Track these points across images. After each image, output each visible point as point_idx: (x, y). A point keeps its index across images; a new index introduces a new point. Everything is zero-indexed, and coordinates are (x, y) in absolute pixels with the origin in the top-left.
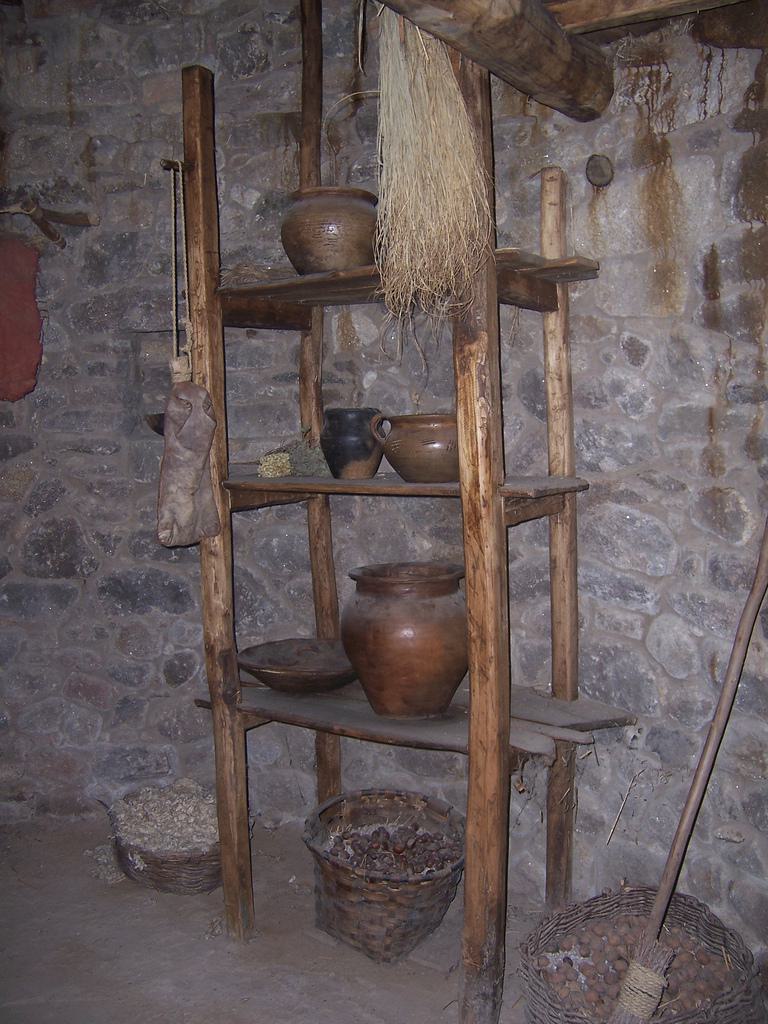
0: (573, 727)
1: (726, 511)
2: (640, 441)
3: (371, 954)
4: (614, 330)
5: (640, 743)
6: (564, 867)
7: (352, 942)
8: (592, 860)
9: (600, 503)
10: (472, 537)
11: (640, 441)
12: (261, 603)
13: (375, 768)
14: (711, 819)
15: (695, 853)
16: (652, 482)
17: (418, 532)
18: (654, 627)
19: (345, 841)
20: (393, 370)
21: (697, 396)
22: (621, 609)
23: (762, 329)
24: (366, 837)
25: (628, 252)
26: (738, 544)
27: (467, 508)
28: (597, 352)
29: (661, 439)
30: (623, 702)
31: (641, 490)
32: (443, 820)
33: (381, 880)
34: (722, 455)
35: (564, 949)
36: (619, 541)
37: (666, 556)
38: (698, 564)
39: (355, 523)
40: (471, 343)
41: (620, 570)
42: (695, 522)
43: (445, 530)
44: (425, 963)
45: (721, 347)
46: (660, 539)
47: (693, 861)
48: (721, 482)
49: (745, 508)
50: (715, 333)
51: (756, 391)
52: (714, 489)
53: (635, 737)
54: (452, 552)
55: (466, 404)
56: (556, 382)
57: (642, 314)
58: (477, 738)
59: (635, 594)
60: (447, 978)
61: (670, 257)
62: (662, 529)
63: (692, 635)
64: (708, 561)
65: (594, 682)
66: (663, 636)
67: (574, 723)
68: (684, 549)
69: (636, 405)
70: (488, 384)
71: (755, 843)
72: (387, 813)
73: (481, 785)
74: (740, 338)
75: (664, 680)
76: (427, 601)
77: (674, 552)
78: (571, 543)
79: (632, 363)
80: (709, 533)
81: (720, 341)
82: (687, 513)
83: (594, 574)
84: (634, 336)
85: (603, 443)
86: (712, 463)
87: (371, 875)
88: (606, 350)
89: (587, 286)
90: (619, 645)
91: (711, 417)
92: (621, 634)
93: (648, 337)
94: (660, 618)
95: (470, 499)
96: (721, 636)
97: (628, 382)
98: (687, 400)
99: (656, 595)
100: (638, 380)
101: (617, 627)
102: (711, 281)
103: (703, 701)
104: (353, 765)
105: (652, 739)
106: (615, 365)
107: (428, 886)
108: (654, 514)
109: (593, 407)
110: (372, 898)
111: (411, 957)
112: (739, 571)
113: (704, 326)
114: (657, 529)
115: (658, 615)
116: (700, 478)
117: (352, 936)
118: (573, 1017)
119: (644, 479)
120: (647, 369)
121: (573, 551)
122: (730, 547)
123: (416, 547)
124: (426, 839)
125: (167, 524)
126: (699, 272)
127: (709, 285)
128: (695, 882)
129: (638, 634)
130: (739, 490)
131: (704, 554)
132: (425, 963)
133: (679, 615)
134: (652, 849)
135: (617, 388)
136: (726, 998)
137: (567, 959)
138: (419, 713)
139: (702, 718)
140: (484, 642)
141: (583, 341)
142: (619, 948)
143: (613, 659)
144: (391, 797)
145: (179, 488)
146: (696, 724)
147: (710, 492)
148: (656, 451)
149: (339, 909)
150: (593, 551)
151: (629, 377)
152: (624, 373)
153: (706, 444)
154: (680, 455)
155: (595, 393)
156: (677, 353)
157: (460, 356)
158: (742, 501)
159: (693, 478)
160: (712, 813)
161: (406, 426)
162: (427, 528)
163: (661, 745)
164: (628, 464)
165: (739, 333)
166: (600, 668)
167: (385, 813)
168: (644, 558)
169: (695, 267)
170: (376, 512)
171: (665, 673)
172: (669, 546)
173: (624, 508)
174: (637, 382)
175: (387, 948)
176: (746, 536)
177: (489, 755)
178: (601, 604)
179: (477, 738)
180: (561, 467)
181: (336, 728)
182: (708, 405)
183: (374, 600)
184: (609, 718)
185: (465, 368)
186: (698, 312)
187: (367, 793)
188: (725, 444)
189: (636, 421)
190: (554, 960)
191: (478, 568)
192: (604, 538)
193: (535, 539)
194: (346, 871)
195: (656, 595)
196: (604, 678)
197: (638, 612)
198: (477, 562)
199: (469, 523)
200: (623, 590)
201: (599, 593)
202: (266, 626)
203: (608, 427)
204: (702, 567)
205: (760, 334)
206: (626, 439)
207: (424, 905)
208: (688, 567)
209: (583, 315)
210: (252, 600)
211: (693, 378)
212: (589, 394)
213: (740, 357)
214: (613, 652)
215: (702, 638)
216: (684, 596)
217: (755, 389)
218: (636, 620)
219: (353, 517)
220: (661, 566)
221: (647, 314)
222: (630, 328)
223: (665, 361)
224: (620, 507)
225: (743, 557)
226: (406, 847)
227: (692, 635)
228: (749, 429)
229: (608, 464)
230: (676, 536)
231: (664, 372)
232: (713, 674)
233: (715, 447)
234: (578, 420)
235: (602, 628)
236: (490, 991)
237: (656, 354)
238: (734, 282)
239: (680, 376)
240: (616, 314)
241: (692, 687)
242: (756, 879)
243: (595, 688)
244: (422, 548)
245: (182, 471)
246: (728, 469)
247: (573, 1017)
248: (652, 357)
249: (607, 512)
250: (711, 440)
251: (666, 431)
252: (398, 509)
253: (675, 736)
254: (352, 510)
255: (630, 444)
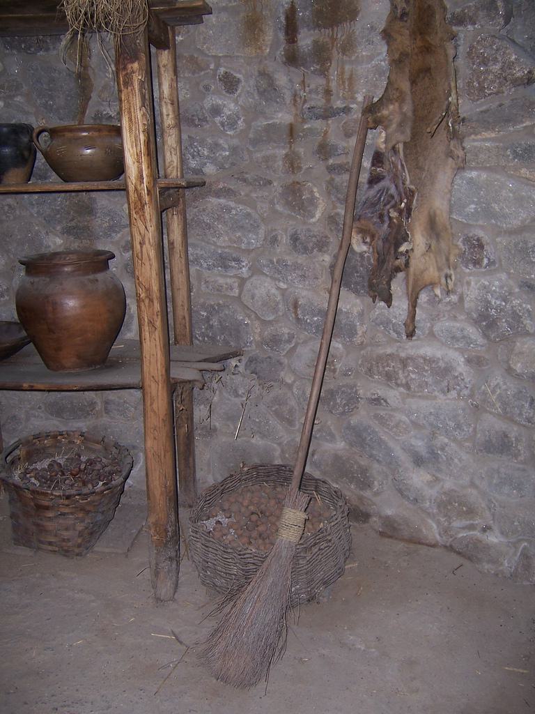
0: (205, 360)
1: (303, 197)
2: (234, 150)
3: (66, 553)
4: (212, 66)
5: (241, 369)
6: (191, 465)
7: (50, 548)
8: (208, 456)
9: (203, 198)
10: (138, 219)
11: (234, 150)
13: (28, 419)
14: (297, 412)
15: (286, 437)
16: (245, 180)
18: (248, 285)
19: (28, 476)
20: (18, 99)
21: (280, 115)
22: (221, 276)
23: (330, 66)
24: (44, 469)
25: (224, 5)
26: (313, 220)
27: (133, 196)
28: (198, 84)
29: (251, 149)
30: (226, 343)
31: (236, 186)
32: (98, 447)
33: (75, 496)
34: (299, 158)
35: (213, 516)
36: (220, 226)
37: (257, 234)
38: (282, 238)
40: (133, 62)
41: (221, 247)
42: (279, 208)
44: (107, 550)
45: (298, 79)
46: (252, 222)
47: (285, 442)
48: (299, 177)
49: (317, 195)
50: (292, 69)
51: (326, 110)
52: (294, 182)
53: (236, 366)
54: (81, 245)
55: (130, 113)
56: (170, 107)
57: (236, 54)
58: (149, 374)
59: (233, 264)
60: (127, 556)
61: (258, 10)
62: (253, 214)
63: (278, 288)
64: (289, 235)
65: (203, 330)
66: (256, 292)
67: (204, 358)
68: (270, 228)
69: (232, 123)
70: (147, 97)
71: (329, 423)
72: (53, 450)
73: (156, 410)
74: (313, 72)
75: (257, 323)
76: (91, 277)
77: (262, 232)
78: (184, 229)
79: (227, 92)
80: (289, 215)
81: (296, 74)
82: (272, 202)
83: (199, 252)
84: (228, 71)
85: (206, 153)
86: (292, 163)
87: (67, 494)
88: (206, 82)
89: (188, 32)
90: (221, 302)
91: (292, 130)
92: (223, 293)
93: (240, 72)
94: (253, 279)
95: (136, 189)
96: (301, 286)
97: (224, 106)
98: (273, 118)
99: (249, 262)
100: (232, 105)
101: (219, 289)
102: (291, 29)
103: (288, 334)
104: (9, 421)
105: (250, 365)
106: (213, 94)
107: (108, 494)
108: (245, 205)
109: (196, 126)
110: (66, 511)
111: (96, 549)
112: (314, 239)
113: (284, 63)
114: (249, 215)
115: (250, 277)
116: (282, 175)
117: (50, 543)
118: (244, 554)
119: (238, 178)
120: (239, 96)
121: (185, 235)
122: (305, 223)
123: (50, 244)
124: (91, 462)
126: (282, 22)
127: (290, 32)
128: (287, 456)
129: (236, 292)
130: (312, 183)
131: (286, 230)
132: (107, 550)
133: (267, 275)
134: (253, 441)
135: (216, 111)
136: (334, 518)
137: (218, 522)
138: (89, 365)
139: (288, 345)
140: (151, 301)
141: (186, 75)
142: (250, 507)
143: (217, 312)
144: (55, 437)
146: (283, 350)
147: (291, 184)
148: (246, 157)
149: (38, 525)
150: (198, 235)
151: (225, 102)
152: (220, 99)
153: (287, 150)
154: (267, 159)
155: (197, 115)
156: (264, 84)
157: (124, 73)
158: (315, 190)
159: (277, 175)
160: (297, 408)
161: (68, 135)
162: (59, 228)
163: (258, 369)
164: (224, 168)
165: (312, 68)
166: (208, 319)
167: (51, 451)
168: (239, 237)
169: (279, 18)
170: (12, 218)
171: (257, 318)
172: (258, 226)
173: (222, 201)
174: (232, 106)
175: (79, 546)
176: (318, 215)
177: (160, 385)
178: (206, 273)
179: (149, 374)
180: (175, 171)
181: (25, 385)
182: (289, 122)
183: (48, 279)
184: (225, 353)
185: (128, 82)
186: (280, 52)
187: (37, 437)
188: (301, 150)
189: (230, 135)
190: (210, 524)
191: (144, 243)
192: (207, 224)
194: (45, 494)
195: (249, 262)
196: (211, 327)
197: (235, 276)
198: (143, 239)
199: (135, 209)
200: (223, 261)
201: (205, 265)
203: (209, 141)
204: (285, 239)
205: (329, 69)
206: (224, 150)
207: (105, 508)
208: (274, 240)
209: (186, 54)
211: (277, 102)
212: (193, 116)
213: (313, 86)
214: (216, 308)
215: (286, 289)
216: (272, 262)
217: (324, 109)
218: (234, 282)
220: (253, 241)
221: (240, 54)
222: (225, 64)
223: (254, 90)
224: (219, 200)
225: (316, 230)
226: (80, 470)
227: (278, 288)
228: (320, 138)
229: (210, 169)
230: (263, 219)
231: (253, 98)
232: (296, 313)
233: (294, 152)
234: (185, 137)
235: (208, 291)
236: (173, 554)
237: (247, 85)
238: (309, 30)
239: (267, 101)
240: (213, 54)
241: (280, 325)
242: (330, 445)
243: (203, 335)
244: (55, 244)
246: (304, 168)
247: (244, 554)
248: (243, 87)
249: (209, 205)
250: (291, 147)
251: (255, 142)
252: (32, 215)
253: (268, 360)
255: (227, 153)
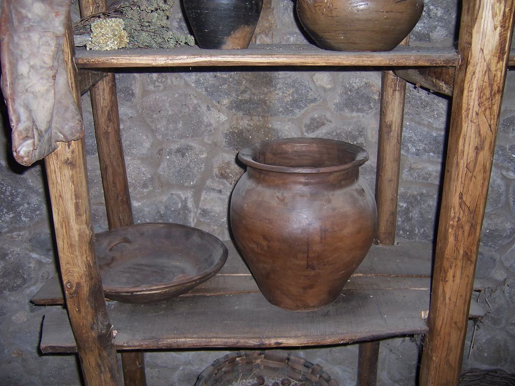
12: (25, 196)
17: (214, 106)
39: (135, 100)
43: (246, 102)
90: (424, 191)
123: (212, 121)
125: (27, 130)
145: (32, 67)
162: (225, 101)
193: (346, 105)
196: (409, 219)
202: (32, 219)
210: (12, 194)
219: (133, 94)
245: (35, 37)
254: (133, 88)
